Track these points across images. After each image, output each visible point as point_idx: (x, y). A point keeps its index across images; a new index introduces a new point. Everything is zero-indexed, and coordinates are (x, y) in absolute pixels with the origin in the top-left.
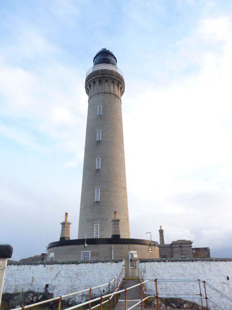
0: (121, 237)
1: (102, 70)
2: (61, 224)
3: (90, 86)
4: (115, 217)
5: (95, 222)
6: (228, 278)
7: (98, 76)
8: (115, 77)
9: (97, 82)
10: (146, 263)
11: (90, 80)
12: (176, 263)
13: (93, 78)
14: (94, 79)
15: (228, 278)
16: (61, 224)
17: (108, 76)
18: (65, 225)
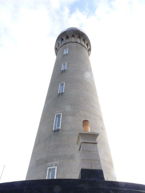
4: (86, 129)
5: (49, 164)
7: (66, 33)
9: (64, 38)
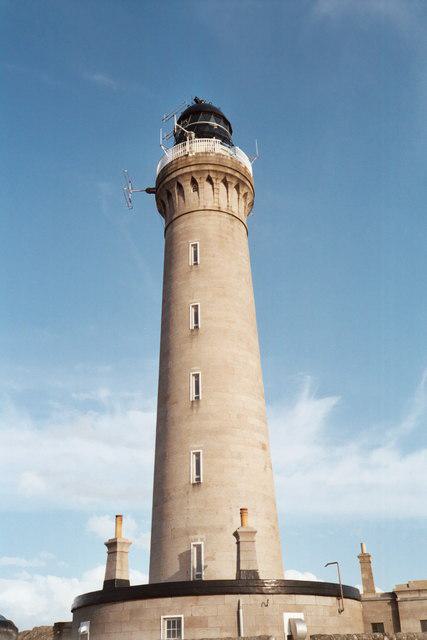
8: (229, 171)
17: (211, 168)
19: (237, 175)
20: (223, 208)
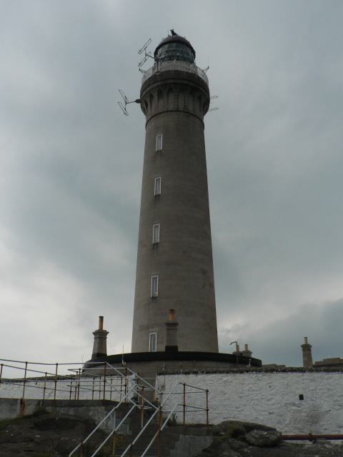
0: (180, 350)
1: (177, 72)
2: (94, 333)
3: (151, 96)
5: (151, 330)
6: (301, 397)
8: (185, 82)
9: (170, 318)
10: (167, 376)
11: (145, 93)
12: (214, 375)
13: (147, 90)
14: (149, 91)
15: (301, 397)
16: (94, 333)
17: (171, 81)
18: (101, 336)
19: (191, 84)
20: (181, 108)
